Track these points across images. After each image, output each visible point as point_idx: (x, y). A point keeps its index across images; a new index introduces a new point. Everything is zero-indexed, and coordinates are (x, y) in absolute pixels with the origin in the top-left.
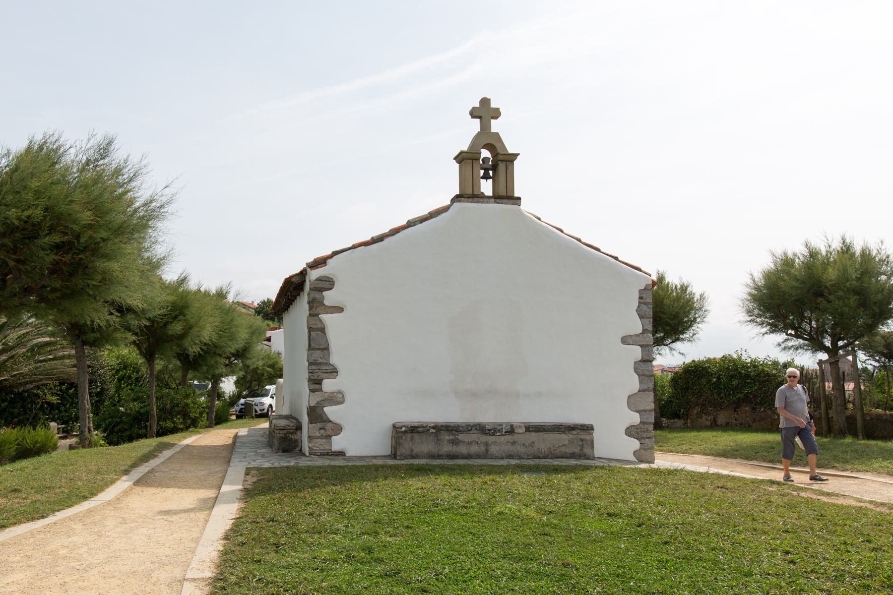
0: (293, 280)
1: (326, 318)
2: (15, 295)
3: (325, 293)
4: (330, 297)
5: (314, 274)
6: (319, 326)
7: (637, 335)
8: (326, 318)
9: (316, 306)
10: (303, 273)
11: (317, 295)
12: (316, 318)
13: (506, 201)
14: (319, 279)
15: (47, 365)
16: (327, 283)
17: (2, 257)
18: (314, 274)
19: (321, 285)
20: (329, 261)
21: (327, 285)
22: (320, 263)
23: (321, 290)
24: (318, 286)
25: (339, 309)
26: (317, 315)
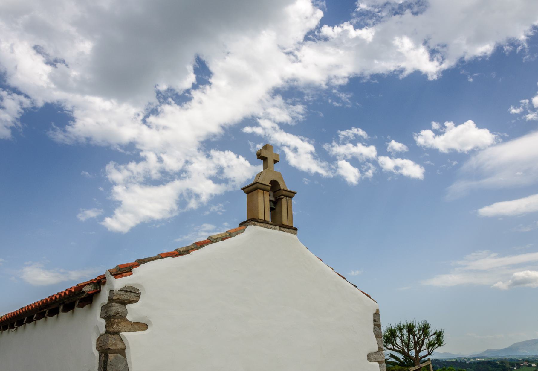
0: (84, 289)
1: (128, 336)
2: (264, 110)
3: (128, 306)
4: (133, 312)
5: (119, 283)
6: (120, 346)
7: (376, 353)
8: (128, 336)
9: (114, 320)
10: (100, 282)
11: (116, 308)
12: (116, 337)
13: (287, 230)
14: (124, 290)
15: (520, 274)
16: (132, 295)
17: (32, 72)
18: (119, 283)
19: (125, 296)
20: (134, 270)
21: (131, 297)
22: (123, 271)
23: (124, 303)
24: (122, 297)
25: (142, 326)
26: (118, 333)
